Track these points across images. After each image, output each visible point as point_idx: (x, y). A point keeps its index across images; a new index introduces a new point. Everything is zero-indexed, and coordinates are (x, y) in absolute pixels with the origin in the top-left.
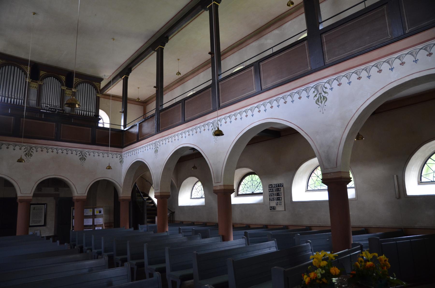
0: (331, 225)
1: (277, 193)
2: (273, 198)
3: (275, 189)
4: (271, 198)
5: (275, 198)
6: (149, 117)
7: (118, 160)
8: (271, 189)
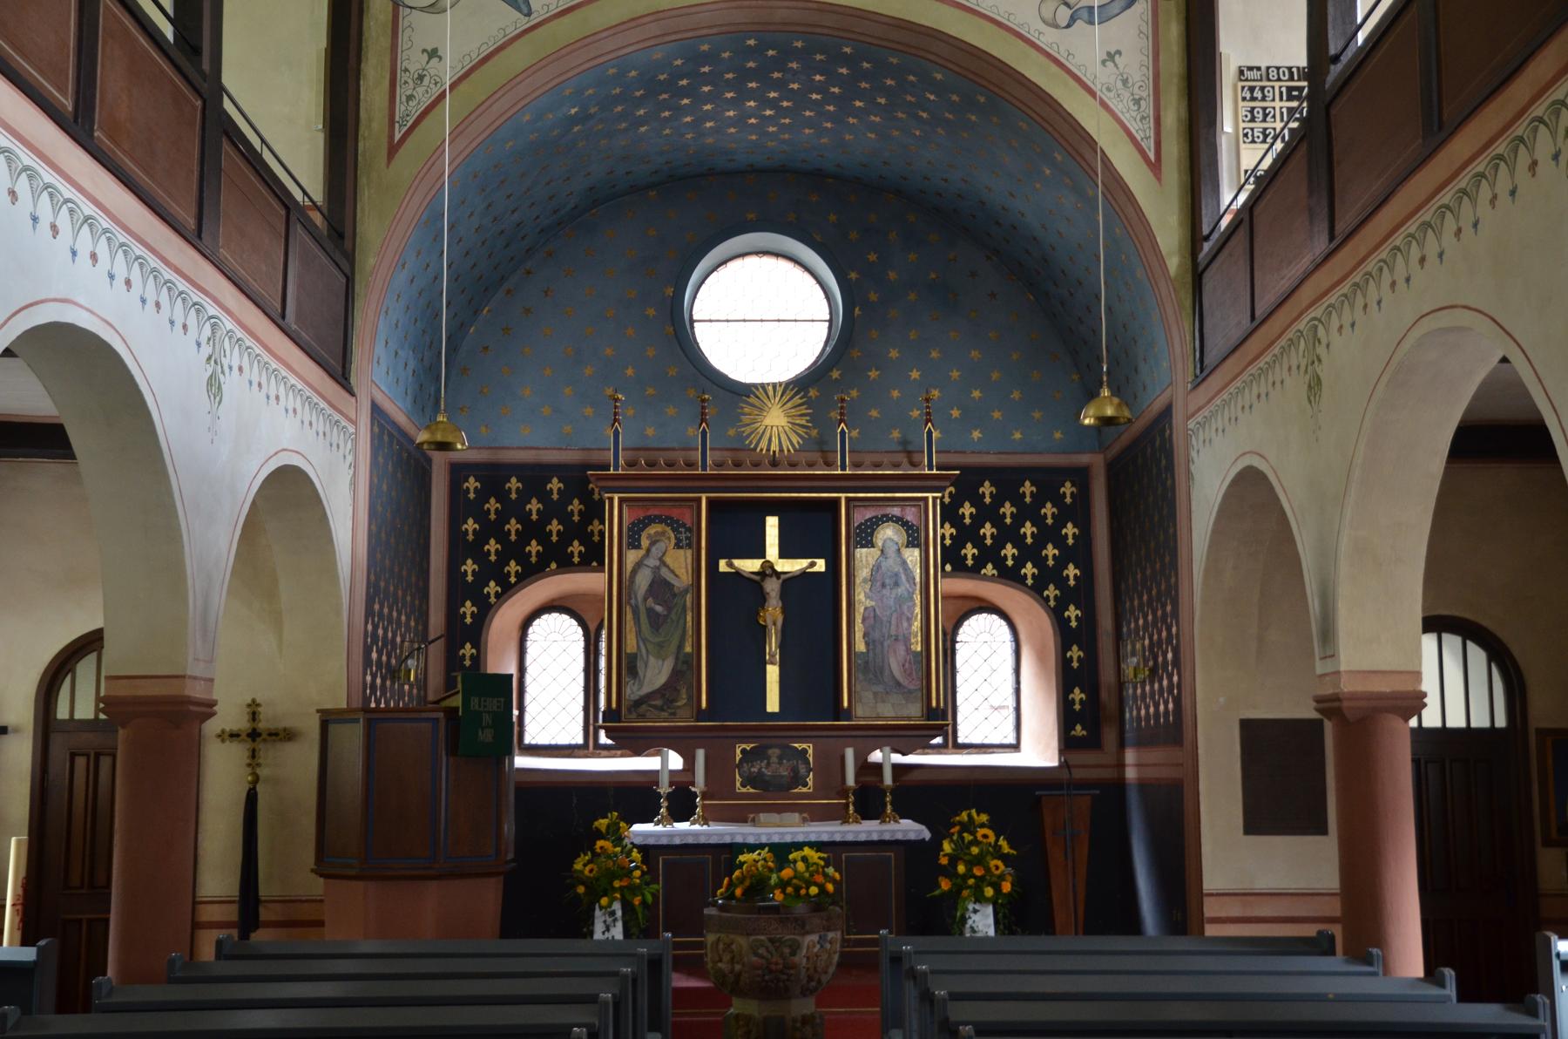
0: (1341, 888)
1: (1288, 109)
2: (1265, 129)
3: (1280, 87)
4: (1252, 129)
5: (1274, 108)
6: (421, 584)
7: (627, 827)
8: (1252, 89)
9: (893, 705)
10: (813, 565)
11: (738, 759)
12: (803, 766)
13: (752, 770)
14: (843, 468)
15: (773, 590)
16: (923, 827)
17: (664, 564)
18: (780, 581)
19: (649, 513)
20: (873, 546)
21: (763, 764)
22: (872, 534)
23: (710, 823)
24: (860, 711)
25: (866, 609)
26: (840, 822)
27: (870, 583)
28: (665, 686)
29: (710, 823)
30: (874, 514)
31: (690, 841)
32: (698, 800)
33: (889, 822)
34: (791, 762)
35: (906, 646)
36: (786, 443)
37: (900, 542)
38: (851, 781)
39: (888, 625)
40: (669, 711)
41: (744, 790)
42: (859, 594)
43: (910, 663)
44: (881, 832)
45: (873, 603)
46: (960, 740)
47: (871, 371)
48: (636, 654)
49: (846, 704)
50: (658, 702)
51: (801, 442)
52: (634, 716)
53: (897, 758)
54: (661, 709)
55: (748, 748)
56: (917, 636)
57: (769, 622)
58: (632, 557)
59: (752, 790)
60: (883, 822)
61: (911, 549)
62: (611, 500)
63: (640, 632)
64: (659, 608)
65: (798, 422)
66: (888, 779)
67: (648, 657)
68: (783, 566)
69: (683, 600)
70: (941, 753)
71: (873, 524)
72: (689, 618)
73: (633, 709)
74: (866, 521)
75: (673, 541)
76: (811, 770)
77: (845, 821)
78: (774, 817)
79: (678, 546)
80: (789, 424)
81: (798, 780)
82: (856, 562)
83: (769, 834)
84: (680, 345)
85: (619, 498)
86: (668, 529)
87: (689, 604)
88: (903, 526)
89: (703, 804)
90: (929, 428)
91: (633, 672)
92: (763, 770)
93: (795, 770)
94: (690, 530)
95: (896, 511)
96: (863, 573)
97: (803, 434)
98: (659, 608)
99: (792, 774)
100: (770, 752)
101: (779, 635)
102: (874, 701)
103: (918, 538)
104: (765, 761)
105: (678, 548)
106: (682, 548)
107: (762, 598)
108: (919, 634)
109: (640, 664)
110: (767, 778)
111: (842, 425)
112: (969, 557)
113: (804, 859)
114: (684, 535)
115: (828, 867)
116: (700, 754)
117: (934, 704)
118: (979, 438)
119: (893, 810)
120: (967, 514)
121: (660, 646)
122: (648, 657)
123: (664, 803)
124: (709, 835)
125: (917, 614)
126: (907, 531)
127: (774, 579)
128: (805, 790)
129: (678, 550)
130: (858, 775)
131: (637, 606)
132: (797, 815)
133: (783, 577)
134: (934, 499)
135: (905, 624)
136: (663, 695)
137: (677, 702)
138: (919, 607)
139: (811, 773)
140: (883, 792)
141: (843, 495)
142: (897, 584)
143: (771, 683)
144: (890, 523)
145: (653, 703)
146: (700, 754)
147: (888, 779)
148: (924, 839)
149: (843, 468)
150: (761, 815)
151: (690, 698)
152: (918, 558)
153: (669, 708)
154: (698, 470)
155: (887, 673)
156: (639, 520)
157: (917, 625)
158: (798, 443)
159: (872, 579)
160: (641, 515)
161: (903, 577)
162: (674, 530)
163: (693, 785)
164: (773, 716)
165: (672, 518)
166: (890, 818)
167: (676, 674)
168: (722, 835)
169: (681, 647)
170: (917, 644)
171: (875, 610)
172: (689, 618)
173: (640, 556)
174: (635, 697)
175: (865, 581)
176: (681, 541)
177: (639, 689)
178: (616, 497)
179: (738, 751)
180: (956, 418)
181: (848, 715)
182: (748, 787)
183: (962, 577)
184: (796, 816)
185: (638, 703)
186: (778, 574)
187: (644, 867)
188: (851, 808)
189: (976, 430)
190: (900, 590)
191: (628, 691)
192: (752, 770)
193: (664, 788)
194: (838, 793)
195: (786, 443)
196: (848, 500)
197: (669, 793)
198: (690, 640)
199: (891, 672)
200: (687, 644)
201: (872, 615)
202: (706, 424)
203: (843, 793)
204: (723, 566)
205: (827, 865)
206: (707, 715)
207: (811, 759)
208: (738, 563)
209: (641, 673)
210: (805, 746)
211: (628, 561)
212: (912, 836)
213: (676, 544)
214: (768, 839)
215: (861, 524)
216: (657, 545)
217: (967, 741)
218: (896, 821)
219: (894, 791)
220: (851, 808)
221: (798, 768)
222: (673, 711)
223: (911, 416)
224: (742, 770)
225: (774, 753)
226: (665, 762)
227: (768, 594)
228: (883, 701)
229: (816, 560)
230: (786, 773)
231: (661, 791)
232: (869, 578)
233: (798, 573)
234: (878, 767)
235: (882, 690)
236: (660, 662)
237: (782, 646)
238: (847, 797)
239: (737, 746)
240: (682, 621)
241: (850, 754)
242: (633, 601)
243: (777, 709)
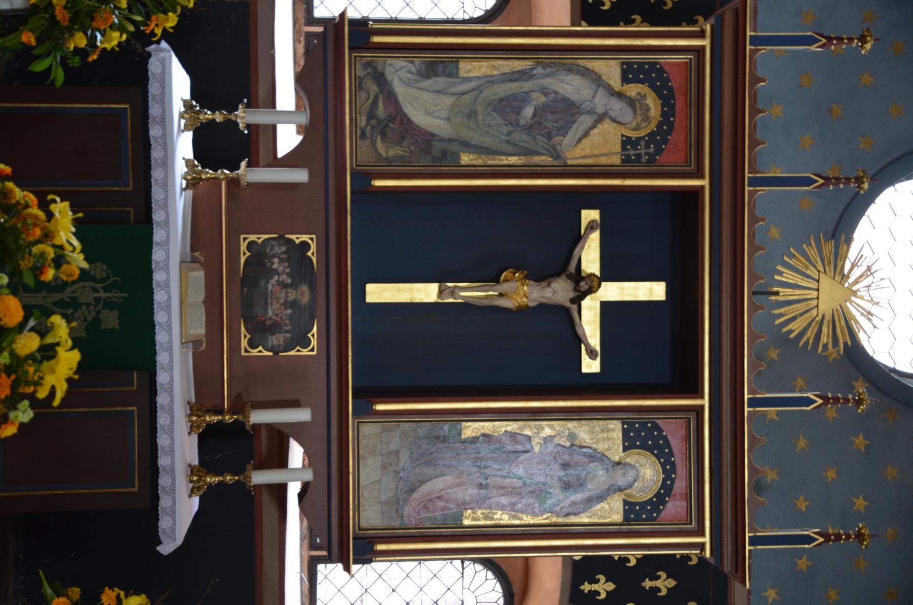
9: (379, 481)
10: (592, 354)
11: (293, 237)
12: (282, 342)
13: (276, 260)
14: (753, 403)
15: (555, 292)
16: (180, 540)
17: (600, 119)
18: (568, 304)
19: (677, 96)
20: (625, 449)
21: (285, 276)
22: (645, 447)
23: (190, 192)
24: (369, 429)
25: (529, 438)
26: (193, 400)
27: (568, 444)
28: (407, 123)
29: (190, 192)
30: (676, 451)
31: (156, 154)
32: (227, 172)
33: (191, 481)
34: (288, 322)
35: (472, 501)
36: (790, 311)
37: (632, 491)
38: (258, 417)
39: (504, 473)
40: (369, 128)
41: (243, 246)
42: (551, 427)
43: (444, 509)
44: (172, 471)
45: (537, 449)
46: (321, 567)
47: (865, 438)
48: (458, 77)
49: (380, 407)
50: (381, 111)
51: (792, 336)
52: (360, 72)
53: (294, 489)
54: (371, 116)
55: (309, 254)
56: (486, 517)
57: (504, 287)
58: (610, 70)
59: (243, 260)
60: (192, 469)
61: (622, 508)
62: (701, 35)
63: (493, 82)
64: (528, 112)
65: (825, 329)
66: (260, 478)
67: (453, 94)
68: (590, 308)
69: (545, 152)
70: (302, 540)
71: (660, 448)
72: (513, 160)
73: (370, 70)
74: (665, 439)
75: (634, 135)
76: (276, 353)
77: (196, 409)
78: (198, 295)
79: (626, 142)
80: (820, 317)
81: (258, 336)
82: (601, 423)
83: (167, 285)
84: (898, 159)
85: (703, 47)
86: (653, 126)
87: (537, 159)
88: (658, 495)
89: (221, 180)
90: (817, 540)
91: (430, 70)
92: (276, 277)
93: (275, 328)
94: (652, 160)
95: (680, 485)
96: (584, 432)
97: (805, 339)
98: (528, 112)
99: (268, 322)
100: (305, 288)
101: (486, 303)
102: (384, 452)
103: (638, 519)
104: (289, 281)
105: (623, 142)
106: (624, 148)
107: (541, 276)
108: (488, 523)
109: (441, 82)
110: (262, 284)
111: (820, 401)
112: (595, 587)
113: (48, 352)
114: (643, 151)
115: (32, 406)
116: (300, 176)
117: (380, 547)
118: (767, 598)
119: (210, 485)
120: (658, 583)
121: (472, 115)
122: (453, 94)
123: (219, 117)
124: (167, 184)
125: (521, 519)
126: (650, 501)
127: (572, 294)
128: (244, 343)
129: (619, 141)
130: (270, 427)
131: (532, 77)
132: (203, 331)
133: (574, 308)
134: (702, 546)
135: (504, 500)
136: (391, 119)
137: (383, 141)
138: (532, 522)
139: (271, 354)
140: (239, 469)
141: (706, 402)
142: (567, 486)
143: (410, 290)
144: (662, 476)
145: (380, 104)
146: (300, 176)
147: (260, 478)
148: (160, 543)
149: (753, 403)
150: (201, 274)
151: (389, 161)
152: (606, 521)
153: (373, 128)
154: (749, 173)
155: (428, 471)
156: (668, 80)
157: (503, 518)
158: (791, 331)
159: (575, 446)
160: (676, 83)
161: (578, 497)
162: (651, 135)
163: (249, 165)
164: (361, 293)
165: (670, 131)
166: (198, 481)
167: (427, 139)
168: (166, 205)
169: (468, 146)
170: (474, 519)
171: (526, 452)
172: (513, 160)
173: (611, 82)
174: (390, 74)
175: (572, 436)
176: (635, 148)
177: (400, 79)
178: (706, 42)
179: (305, 238)
180: (796, 564)
181: (365, 412)
182: (248, 254)
183: (563, 577)
184: (199, 330)
185: (380, 78)
186: (577, 300)
187: (95, 57)
188: (215, 418)
189: (777, 594)
190: (557, 493)
191: (399, 63)
192: (276, 260)
193: (244, 117)
194: (239, 395)
195: (790, 311)
196: (699, 410)
197: (237, 124)
198: (480, 162)
199: (430, 479)
200: (471, 156)
201: (519, 448)
202: (822, 184)
203: (240, 406)
204: (590, 215)
205: (35, 403)
206: (363, 192)
207: (292, 353)
208: (594, 239)
209: (427, 83)
210: (314, 342)
211: (601, 63)
212: (164, 523)
213: (629, 138)
214: (158, 283)
215: (660, 431)
216: (628, 110)
217: (320, 577)
218: (192, 493)
219: (241, 488)
220: (215, 418)
221: (280, 333)
222: (368, 134)
223: (798, 499)
224: (275, 243)
225: (303, 295)
226: (286, 116)
227: (549, 285)
228: (384, 467)
229: (598, 359)
230: (270, 313)
231: (240, 112)
232: (577, 443)
233: (579, 332)
234: (281, 461)
235: (401, 464)
236: (444, 114)
237: (467, 307)
238: (232, 411)
239: (314, 236)
240: (509, 149)
241: (302, 415)
242: (539, 70)
243: (370, 299)
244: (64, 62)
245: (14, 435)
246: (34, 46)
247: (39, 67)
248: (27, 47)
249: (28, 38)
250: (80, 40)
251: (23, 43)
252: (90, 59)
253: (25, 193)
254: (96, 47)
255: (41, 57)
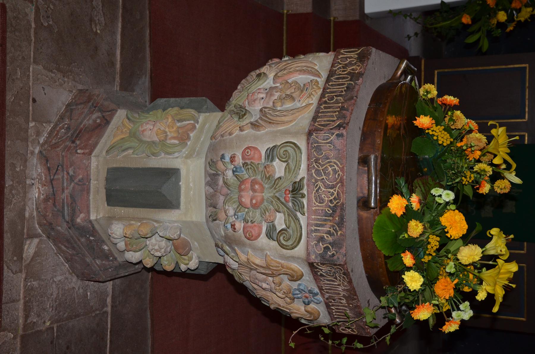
115: (472, 307)
205: (475, 305)
244: (489, 33)
245: (456, 330)
246: (470, 24)
247: (471, 40)
248: (466, 26)
249: (466, 19)
250: (502, 16)
251: (463, 23)
252: (508, 30)
253: (469, 120)
254: (514, 21)
255: (473, 33)
